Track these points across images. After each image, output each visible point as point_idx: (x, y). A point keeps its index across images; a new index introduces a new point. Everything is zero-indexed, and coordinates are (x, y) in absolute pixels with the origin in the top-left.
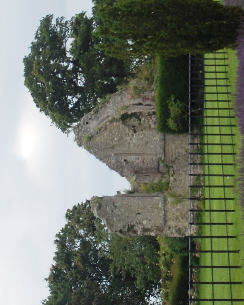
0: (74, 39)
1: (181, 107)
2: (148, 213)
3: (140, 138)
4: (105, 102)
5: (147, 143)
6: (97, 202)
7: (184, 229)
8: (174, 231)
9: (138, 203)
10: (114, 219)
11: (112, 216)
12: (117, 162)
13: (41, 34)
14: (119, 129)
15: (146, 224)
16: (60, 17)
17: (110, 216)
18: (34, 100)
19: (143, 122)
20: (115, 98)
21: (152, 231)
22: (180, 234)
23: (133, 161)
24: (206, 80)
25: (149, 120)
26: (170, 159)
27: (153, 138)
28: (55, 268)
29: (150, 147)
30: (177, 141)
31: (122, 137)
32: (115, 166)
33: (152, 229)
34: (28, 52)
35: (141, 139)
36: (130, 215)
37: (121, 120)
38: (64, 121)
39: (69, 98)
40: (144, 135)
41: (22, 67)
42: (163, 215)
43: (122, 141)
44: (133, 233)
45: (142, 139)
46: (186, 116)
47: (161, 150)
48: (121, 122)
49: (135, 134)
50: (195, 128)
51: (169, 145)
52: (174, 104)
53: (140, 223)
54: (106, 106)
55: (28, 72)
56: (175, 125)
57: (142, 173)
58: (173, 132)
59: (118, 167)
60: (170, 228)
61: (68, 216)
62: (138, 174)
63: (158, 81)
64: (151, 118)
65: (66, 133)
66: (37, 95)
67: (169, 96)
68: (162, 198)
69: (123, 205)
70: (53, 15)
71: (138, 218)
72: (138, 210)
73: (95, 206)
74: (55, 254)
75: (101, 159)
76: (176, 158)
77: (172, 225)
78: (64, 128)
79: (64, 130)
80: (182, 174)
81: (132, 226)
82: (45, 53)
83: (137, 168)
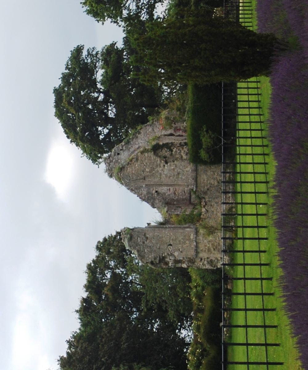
2: (180, 244)
3: (171, 169)
4: (136, 133)
5: (179, 174)
7: (216, 261)
8: (206, 262)
9: (170, 234)
12: (148, 193)
14: (151, 160)
15: (177, 256)
16: (91, 48)
17: (142, 247)
19: (175, 153)
21: (184, 262)
23: (164, 192)
25: (181, 151)
26: (203, 189)
27: (185, 168)
28: (85, 300)
30: (209, 171)
32: (147, 197)
33: (184, 260)
35: (172, 170)
36: (162, 247)
39: (100, 128)
40: (176, 166)
41: (52, 98)
42: (195, 247)
43: (154, 172)
44: (164, 265)
45: (174, 169)
46: (218, 147)
47: (193, 181)
48: (153, 153)
49: (166, 165)
53: (172, 255)
57: (174, 204)
58: (205, 163)
60: (201, 259)
61: (98, 248)
64: (183, 148)
65: (96, 164)
68: (194, 229)
69: (154, 236)
70: (83, 45)
71: (170, 249)
75: (132, 190)
76: (208, 189)
78: (95, 159)
80: (214, 205)
81: (164, 258)
83: (169, 200)
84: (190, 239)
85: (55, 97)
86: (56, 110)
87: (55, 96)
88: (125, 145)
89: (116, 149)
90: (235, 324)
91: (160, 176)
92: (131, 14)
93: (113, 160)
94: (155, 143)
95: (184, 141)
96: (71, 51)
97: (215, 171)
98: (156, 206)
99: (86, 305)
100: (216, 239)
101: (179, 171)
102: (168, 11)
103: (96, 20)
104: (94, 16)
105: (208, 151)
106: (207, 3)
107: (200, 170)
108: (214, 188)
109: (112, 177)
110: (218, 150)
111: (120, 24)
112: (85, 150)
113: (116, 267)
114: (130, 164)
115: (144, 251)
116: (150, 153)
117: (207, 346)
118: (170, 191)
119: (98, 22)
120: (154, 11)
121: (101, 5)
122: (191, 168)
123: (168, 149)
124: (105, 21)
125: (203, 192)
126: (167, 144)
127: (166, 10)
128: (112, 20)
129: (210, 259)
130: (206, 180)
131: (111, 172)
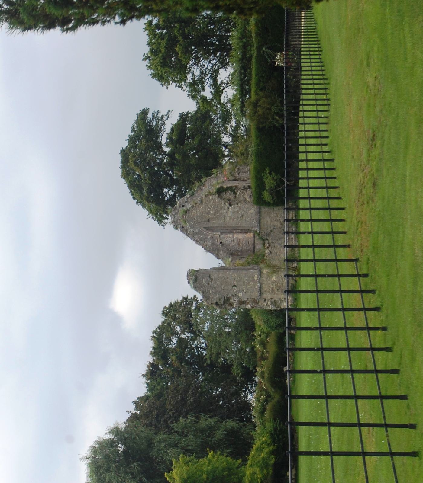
0: (170, 149)
1: (276, 180)
2: (244, 285)
3: (235, 212)
4: (201, 185)
5: (242, 216)
6: (193, 275)
7: (280, 301)
8: (269, 303)
9: (234, 275)
10: (211, 291)
11: (208, 288)
12: (213, 244)
13: (137, 127)
14: (215, 202)
15: (241, 297)
16: (156, 111)
17: (206, 288)
18: (131, 192)
19: (239, 195)
20: (210, 181)
21: (248, 303)
22: (275, 306)
23: (229, 243)
24: (300, 172)
25: (244, 194)
26: (266, 231)
27: (249, 211)
28: (152, 365)
29: (246, 220)
30: (272, 214)
31: (218, 211)
32: (211, 248)
33: (248, 301)
34: (125, 144)
35: (236, 213)
36: (226, 288)
37: (216, 193)
38: (161, 212)
39: (165, 190)
40: (240, 208)
41: (119, 159)
42: (259, 288)
43: (218, 214)
44: (229, 306)
45: (237, 212)
46: (281, 188)
47: (257, 222)
48: (217, 195)
49: (230, 208)
50: (290, 201)
51: (264, 218)
52: (269, 176)
53: (236, 296)
54: (202, 190)
55: (125, 164)
56: (270, 197)
57: (238, 255)
58: (268, 204)
59: (214, 249)
60: (265, 300)
61: (165, 314)
62: (234, 256)
63: (253, 154)
64: (246, 191)
65: (162, 225)
66: (134, 187)
67: (265, 169)
68: (258, 270)
69: (219, 277)
70: (149, 108)
71: (234, 290)
72: (234, 283)
73: (191, 278)
74: (152, 348)
75: (197, 242)
76: (271, 231)
77: (267, 297)
78: (160, 220)
79: (160, 222)
80: (277, 246)
81: (228, 299)
82: (141, 146)
83: (233, 251)
84: (254, 280)
85: (121, 158)
86: (122, 171)
87: (121, 157)
88: (189, 197)
89: (181, 201)
90: (298, 368)
91: (225, 218)
92: (196, 79)
93: (178, 212)
94: (219, 186)
95: (248, 185)
96: (137, 114)
97: (278, 213)
98: (221, 257)
99: (152, 369)
100: (279, 280)
101: (242, 213)
102: (232, 76)
103: (160, 84)
104: (159, 80)
105: (271, 191)
106: (269, 48)
107: (263, 212)
108: (277, 230)
109: (177, 229)
110: (281, 192)
111: (184, 89)
112: (151, 210)
113: (183, 332)
114: (195, 207)
115: (209, 292)
116: (214, 195)
117: (271, 390)
118: (234, 242)
119: (163, 86)
120: (217, 77)
121: (166, 68)
122: (255, 210)
123: (232, 192)
124: (169, 85)
125: (266, 234)
126: (231, 187)
127: (229, 75)
128: (177, 84)
129: (274, 299)
130: (269, 222)
131: (177, 224)
